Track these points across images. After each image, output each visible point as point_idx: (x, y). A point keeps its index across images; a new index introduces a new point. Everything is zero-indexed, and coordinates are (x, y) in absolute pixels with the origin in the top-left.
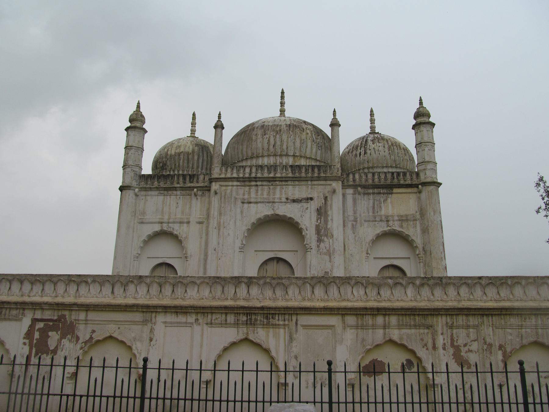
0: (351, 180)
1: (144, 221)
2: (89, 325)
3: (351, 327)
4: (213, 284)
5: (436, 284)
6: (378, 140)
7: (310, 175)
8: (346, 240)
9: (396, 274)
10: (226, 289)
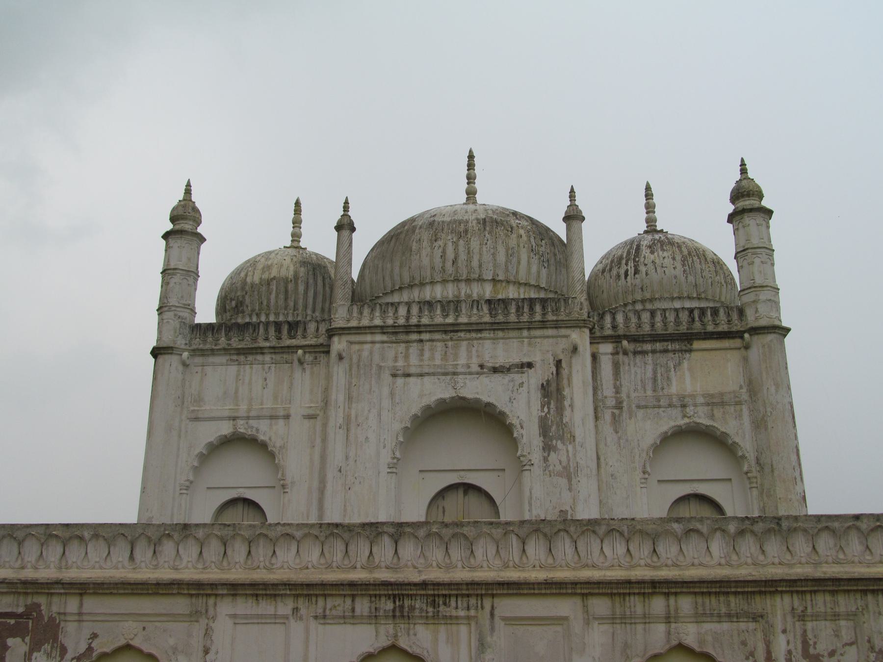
0: (609, 326)
1: (200, 416)
2: (84, 624)
3: (601, 619)
4: (326, 537)
5: (769, 531)
6: (662, 246)
7: (525, 318)
8: (602, 446)
9: (706, 512)
10: (352, 547)
